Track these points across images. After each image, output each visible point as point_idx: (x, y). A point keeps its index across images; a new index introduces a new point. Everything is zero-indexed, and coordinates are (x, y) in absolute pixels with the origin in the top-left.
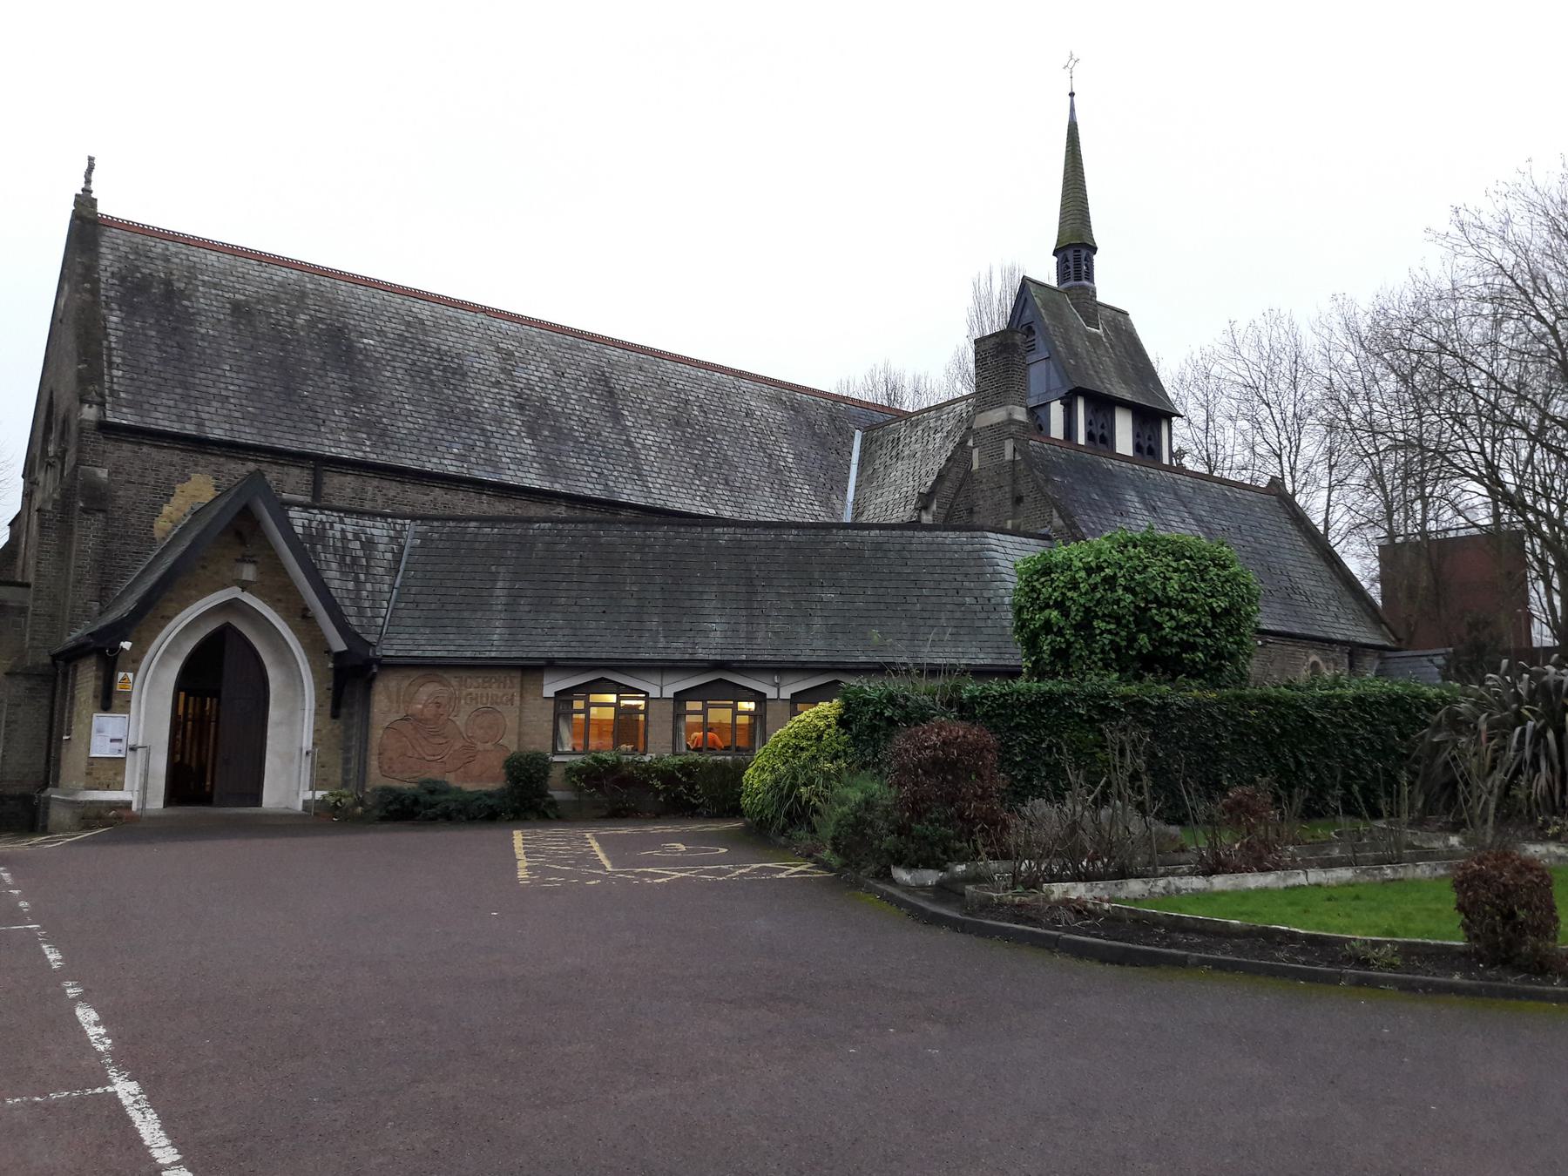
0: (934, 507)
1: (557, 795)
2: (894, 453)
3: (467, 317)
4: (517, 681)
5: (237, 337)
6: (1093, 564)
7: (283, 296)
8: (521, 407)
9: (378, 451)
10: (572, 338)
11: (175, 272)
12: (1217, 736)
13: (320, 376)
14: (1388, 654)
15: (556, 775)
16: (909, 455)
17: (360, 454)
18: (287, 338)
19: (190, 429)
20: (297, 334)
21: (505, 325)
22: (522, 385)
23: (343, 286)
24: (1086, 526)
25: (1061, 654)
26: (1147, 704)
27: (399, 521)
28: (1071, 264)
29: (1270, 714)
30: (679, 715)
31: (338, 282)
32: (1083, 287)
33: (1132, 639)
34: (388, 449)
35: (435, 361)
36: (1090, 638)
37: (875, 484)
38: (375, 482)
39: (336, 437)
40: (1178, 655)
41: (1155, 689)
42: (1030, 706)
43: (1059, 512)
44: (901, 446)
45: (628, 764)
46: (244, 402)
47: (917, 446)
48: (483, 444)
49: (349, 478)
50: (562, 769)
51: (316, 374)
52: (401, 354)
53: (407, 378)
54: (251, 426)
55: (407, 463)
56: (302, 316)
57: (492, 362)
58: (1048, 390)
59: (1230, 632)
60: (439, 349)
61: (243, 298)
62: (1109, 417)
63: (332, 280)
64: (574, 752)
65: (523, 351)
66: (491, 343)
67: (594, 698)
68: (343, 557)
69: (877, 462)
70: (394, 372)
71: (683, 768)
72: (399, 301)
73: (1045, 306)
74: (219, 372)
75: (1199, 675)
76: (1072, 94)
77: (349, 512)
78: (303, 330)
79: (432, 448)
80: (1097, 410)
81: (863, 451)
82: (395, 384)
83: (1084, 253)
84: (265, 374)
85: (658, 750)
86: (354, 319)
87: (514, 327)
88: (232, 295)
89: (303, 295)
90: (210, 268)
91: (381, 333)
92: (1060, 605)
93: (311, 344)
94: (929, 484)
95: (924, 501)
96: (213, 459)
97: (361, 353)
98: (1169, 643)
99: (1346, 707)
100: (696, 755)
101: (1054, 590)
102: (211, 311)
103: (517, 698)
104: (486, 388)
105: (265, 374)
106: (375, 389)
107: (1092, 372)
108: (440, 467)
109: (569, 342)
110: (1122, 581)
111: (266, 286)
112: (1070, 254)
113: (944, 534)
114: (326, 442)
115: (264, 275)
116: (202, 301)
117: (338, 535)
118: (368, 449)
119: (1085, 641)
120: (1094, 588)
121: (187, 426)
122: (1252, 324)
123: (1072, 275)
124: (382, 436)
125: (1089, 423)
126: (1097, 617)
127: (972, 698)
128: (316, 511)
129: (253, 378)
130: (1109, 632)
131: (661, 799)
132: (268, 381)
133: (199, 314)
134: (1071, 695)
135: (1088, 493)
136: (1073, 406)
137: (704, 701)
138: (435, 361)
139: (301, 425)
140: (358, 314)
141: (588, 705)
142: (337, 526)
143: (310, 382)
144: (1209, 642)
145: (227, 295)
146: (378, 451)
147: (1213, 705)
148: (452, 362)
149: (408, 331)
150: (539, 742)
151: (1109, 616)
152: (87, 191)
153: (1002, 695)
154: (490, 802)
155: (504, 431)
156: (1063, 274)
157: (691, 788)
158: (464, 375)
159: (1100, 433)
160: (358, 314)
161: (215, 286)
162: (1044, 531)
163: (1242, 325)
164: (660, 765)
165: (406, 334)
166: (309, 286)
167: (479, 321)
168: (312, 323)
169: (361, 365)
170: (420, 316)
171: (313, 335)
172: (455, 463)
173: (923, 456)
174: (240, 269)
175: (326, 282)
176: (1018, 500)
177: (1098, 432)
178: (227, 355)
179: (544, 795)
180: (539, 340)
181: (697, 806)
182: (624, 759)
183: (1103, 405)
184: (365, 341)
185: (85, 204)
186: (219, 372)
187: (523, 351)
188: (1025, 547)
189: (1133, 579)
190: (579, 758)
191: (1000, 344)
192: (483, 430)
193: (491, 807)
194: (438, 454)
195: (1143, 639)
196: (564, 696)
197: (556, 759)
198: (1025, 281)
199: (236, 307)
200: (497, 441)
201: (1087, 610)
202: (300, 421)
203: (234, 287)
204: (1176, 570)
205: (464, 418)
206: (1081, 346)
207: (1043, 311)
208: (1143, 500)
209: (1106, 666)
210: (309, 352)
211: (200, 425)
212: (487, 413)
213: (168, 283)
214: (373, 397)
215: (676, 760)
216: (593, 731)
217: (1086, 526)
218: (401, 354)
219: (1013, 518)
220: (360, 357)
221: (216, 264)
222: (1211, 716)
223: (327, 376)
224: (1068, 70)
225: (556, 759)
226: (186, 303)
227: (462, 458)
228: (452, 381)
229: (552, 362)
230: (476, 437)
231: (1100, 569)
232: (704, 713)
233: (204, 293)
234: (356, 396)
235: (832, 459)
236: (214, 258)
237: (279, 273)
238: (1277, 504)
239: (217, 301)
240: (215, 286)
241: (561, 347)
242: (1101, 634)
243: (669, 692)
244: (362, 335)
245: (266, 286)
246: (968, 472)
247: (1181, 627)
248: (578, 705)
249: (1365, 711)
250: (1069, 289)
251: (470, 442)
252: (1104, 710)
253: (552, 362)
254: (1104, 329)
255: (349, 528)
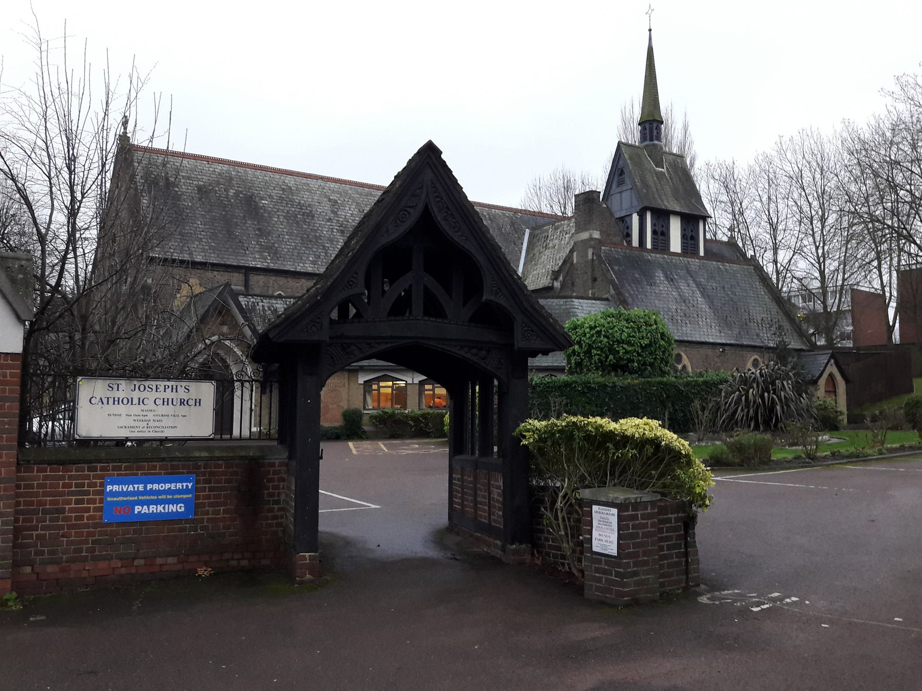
0: (561, 278)
1: (366, 428)
2: (544, 245)
3: (312, 182)
4: (346, 376)
5: (202, 206)
6: (593, 325)
7: (221, 180)
8: (342, 232)
9: (274, 262)
10: (367, 189)
11: (169, 172)
12: (638, 398)
13: (243, 224)
14: (803, 353)
15: (365, 419)
16: (552, 247)
17: (266, 264)
18: (226, 204)
19: (186, 257)
20: (230, 201)
21: (332, 185)
22: (342, 219)
23: (249, 171)
24: (629, 293)
25: (579, 364)
26: (607, 386)
27: (288, 300)
28: (648, 132)
29: (662, 389)
30: (421, 392)
31: (247, 169)
32: (654, 145)
33: (607, 357)
34: (278, 260)
35: (298, 210)
36: (590, 357)
37: (533, 263)
38: (274, 278)
39: (254, 256)
40: (627, 364)
41: (615, 380)
42: (560, 387)
43: (613, 287)
44: (548, 241)
45: (398, 414)
46: (209, 240)
47: (557, 241)
48: (324, 254)
49: (261, 277)
50: (368, 416)
51: (241, 223)
52: (281, 208)
53: (285, 221)
54: (214, 253)
55: (287, 268)
56: (231, 191)
57: (326, 207)
58: (632, 207)
59: (651, 354)
60: (300, 203)
61: (202, 183)
62: (666, 220)
63: (244, 169)
64: (374, 409)
65: (342, 199)
66: (326, 196)
67: (382, 384)
68: (264, 320)
69: (536, 249)
70: (278, 218)
71: (424, 416)
72: (278, 177)
73: (631, 158)
74: (196, 225)
75: (636, 372)
76: (650, 30)
77: (265, 297)
78: (233, 198)
79: (299, 258)
80: (659, 218)
81: (529, 242)
82: (279, 224)
83: (655, 125)
84: (217, 225)
85: (412, 407)
86: (257, 190)
87: (337, 186)
88: (197, 182)
89: (231, 179)
90: (185, 168)
91: (270, 196)
92: (579, 343)
93: (238, 206)
94: (560, 264)
95: (555, 275)
96: (198, 271)
97: (261, 209)
98: (623, 359)
99: (699, 385)
100: (429, 410)
101: (577, 337)
102: (189, 193)
103: (347, 384)
104: (324, 223)
105: (217, 225)
106: (270, 228)
107: (657, 196)
108: (304, 268)
109: (366, 192)
110: (603, 333)
111: (212, 176)
112: (647, 126)
113: (552, 300)
114: (250, 259)
115: (211, 169)
116: (185, 188)
117: (261, 308)
118: (269, 261)
119: (589, 358)
120: (592, 336)
121: (185, 255)
122: (791, 140)
123: (648, 138)
124: (275, 254)
125: (653, 225)
126: (593, 348)
127: (536, 384)
128: (250, 297)
129: (212, 227)
130: (598, 355)
131: (413, 430)
132: (219, 228)
133: (183, 194)
134: (576, 382)
135: (633, 274)
136: (644, 218)
137: (433, 385)
138: (298, 210)
139: (237, 251)
140: (258, 187)
141: (379, 387)
142: (261, 304)
143: (239, 227)
144: (640, 358)
145: (194, 183)
146: (274, 262)
147: (636, 386)
148: (307, 209)
149: (283, 194)
150: (357, 404)
151: (598, 347)
152: (125, 133)
153: (548, 383)
154: (336, 431)
155: (334, 246)
156: (643, 138)
157: (427, 425)
158: (313, 216)
159: (661, 230)
160: (258, 187)
161: (189, 178)
162: (605, 296)
163: (786, 139)
164: (413, 414)
165: (283, 196)
166: (233, 173)
167: (319, 184)
168: (237, 194)
169: (262, 216)
170: (289, 185)
171: (237, 201)
172: (311, 265)
173: (559, 248)
174: (199, 167)
175: (241, 170)
176: (595, 280)
177: (659, 230)
178: (199, 216)
179: (360, 428)
180: (350, 192)
181: (430, 433)
182: (396, 412)
183: (662, 216)
184: (263, 202)
185: (123, 140)
186: (196, 225)
187: (342, 199)
188: (594, 305)
189: (608, 332)
190: (375, 411)
191: (586, 198)
192: (324, 246)
193: (336, 433)
194: (303, 261)
195: (611, 357)
196: (368, 383)
197: (365, 412)
198: (620, 144)
199: (200, 189)
200: (331, 252)
201: (590, 345)
202: (236, 249)
203: (197, 178)
204: (627, 328)
205: (314, 240)
206: (651, 180)
207: (629, 161)
208: (667, 277)
209: (597, 369)
210: (237, 211)
211: (191, 254)
212: (325, 236)
213: (167, 179)
214: (269, 233)
215: (419, 412)
216: (382, 398)
217: (629, 293)
218: (281, 208)
219: (592, 288)
220: (261, 211)
221: (187, 166)
222: (635, 390)
223: (246, 223)
224: (648, 15)
225: (365, 412)
226: (176, 189)
227: (314, 263)
228: (307, 220)
229: (357, 203)
230: (321, 251)
231: (596, 327)
232: (433, 390)
233: (184, 183)
234: (262, 233)
235: (511, 248)
236: (186, 162)
237: (218, 167)
238: (753, 271)
239: (190, 186)
240: (189, 178)
241: (362, 194)
242: (595, 355)
243: (416, 381)
244: (262, 199)
245: (212, 176)
246: (572, 263)
247: (627, 352)
248: (375, 387)
249: (708, 387)
250: (647, 146)
251: (318, 253)
252: (589, 388)
253: (357, 203)
254: (667, 168)
255: (266, 305)
